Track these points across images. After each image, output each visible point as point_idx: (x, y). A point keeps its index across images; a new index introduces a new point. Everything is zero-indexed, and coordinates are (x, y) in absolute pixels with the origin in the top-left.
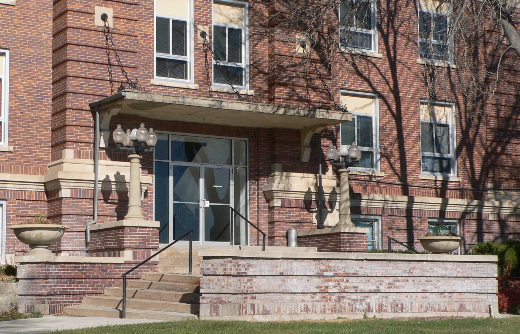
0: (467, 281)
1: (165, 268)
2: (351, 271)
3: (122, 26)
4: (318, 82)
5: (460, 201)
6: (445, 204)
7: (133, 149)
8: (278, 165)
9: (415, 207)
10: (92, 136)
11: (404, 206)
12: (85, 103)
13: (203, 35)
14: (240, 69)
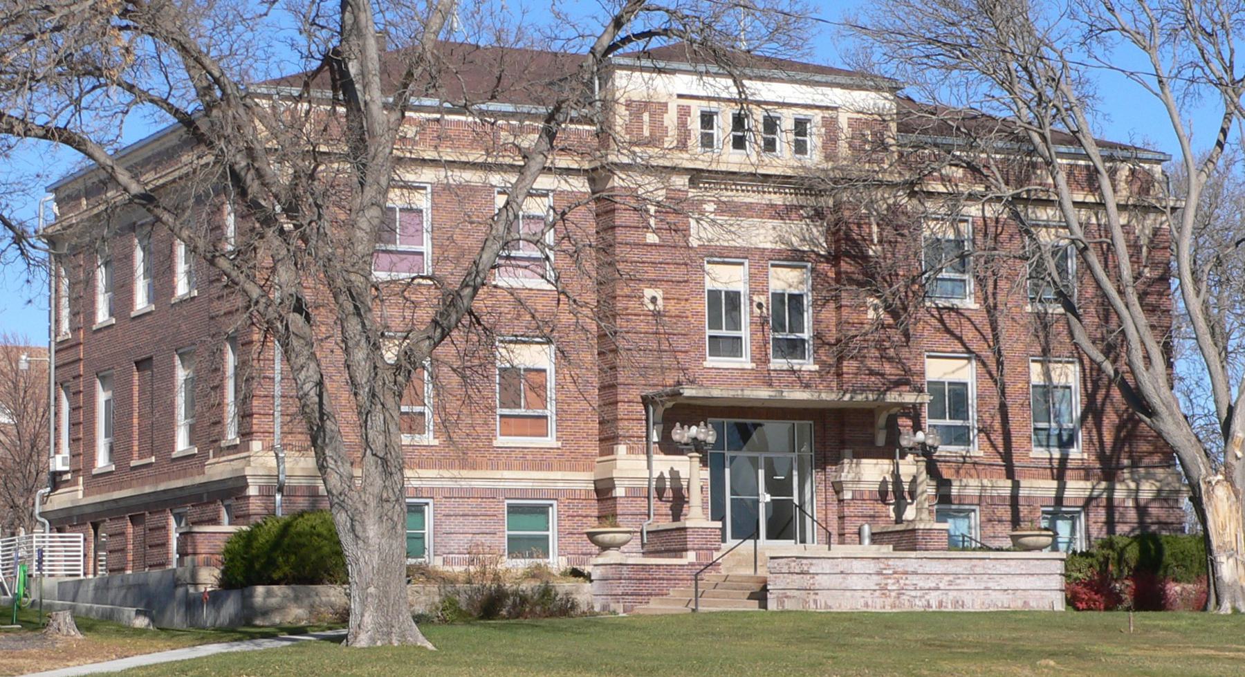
0: (1031, 578)
1: (728, 569)
2: (910, 569)
3: (673, 308)
4: (891, 352)
5: (1082, 484)
6: (1061, 488)
7: (692, 447)
8: (848, 452)
9: (1022, 493)
10: (644, 429)
11: (1007, 492)
12: (635, 394)
13: (760, 306)
14: (803, 341)
